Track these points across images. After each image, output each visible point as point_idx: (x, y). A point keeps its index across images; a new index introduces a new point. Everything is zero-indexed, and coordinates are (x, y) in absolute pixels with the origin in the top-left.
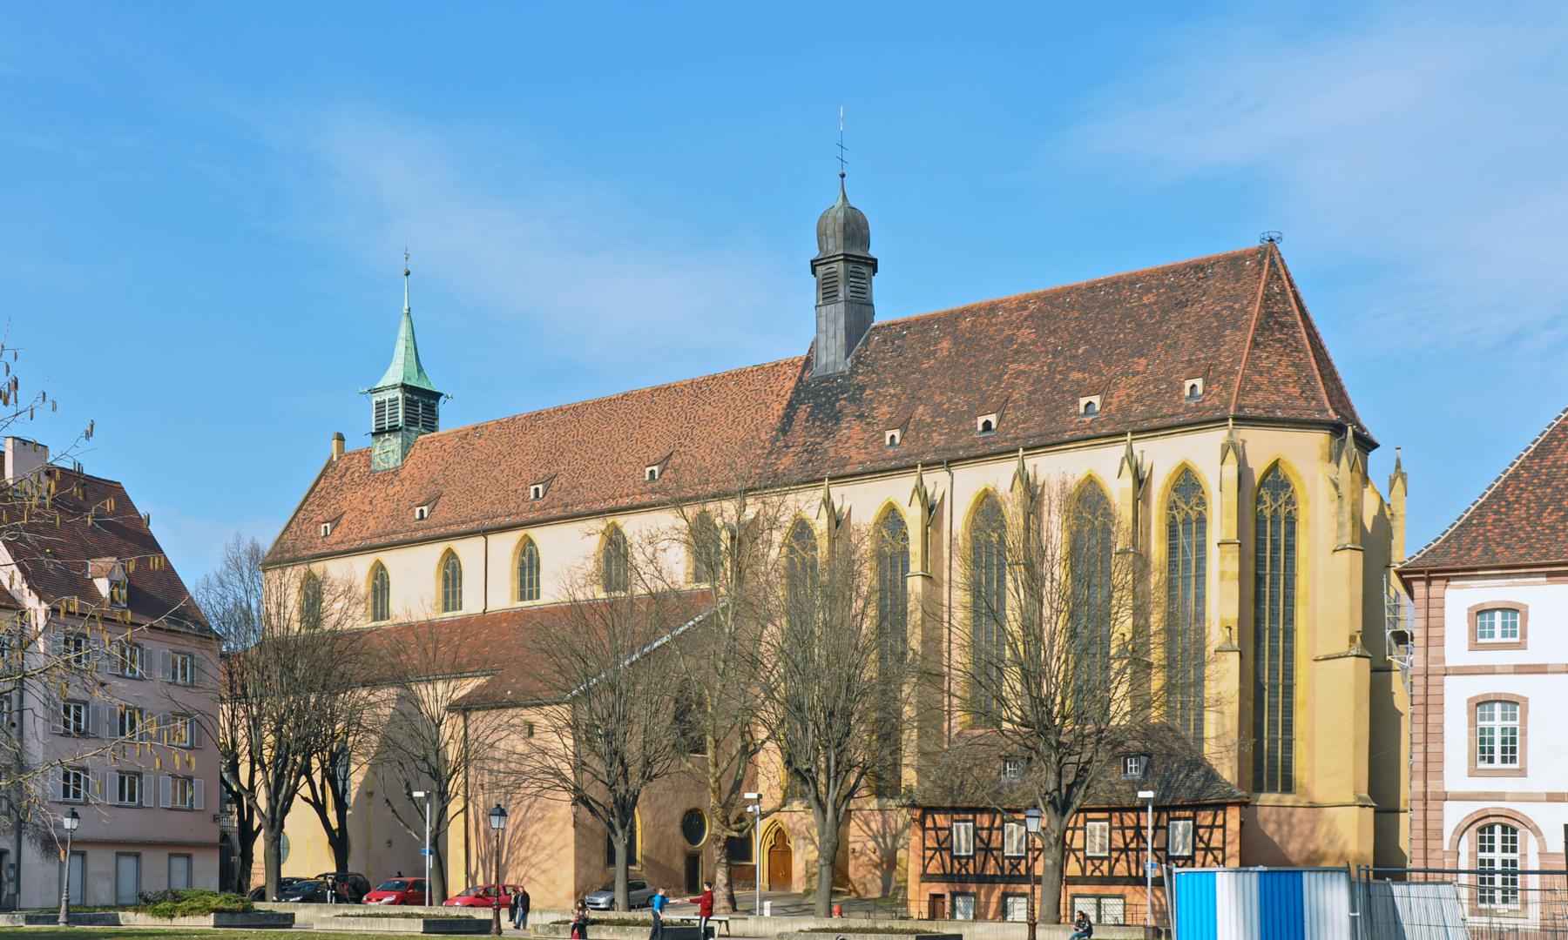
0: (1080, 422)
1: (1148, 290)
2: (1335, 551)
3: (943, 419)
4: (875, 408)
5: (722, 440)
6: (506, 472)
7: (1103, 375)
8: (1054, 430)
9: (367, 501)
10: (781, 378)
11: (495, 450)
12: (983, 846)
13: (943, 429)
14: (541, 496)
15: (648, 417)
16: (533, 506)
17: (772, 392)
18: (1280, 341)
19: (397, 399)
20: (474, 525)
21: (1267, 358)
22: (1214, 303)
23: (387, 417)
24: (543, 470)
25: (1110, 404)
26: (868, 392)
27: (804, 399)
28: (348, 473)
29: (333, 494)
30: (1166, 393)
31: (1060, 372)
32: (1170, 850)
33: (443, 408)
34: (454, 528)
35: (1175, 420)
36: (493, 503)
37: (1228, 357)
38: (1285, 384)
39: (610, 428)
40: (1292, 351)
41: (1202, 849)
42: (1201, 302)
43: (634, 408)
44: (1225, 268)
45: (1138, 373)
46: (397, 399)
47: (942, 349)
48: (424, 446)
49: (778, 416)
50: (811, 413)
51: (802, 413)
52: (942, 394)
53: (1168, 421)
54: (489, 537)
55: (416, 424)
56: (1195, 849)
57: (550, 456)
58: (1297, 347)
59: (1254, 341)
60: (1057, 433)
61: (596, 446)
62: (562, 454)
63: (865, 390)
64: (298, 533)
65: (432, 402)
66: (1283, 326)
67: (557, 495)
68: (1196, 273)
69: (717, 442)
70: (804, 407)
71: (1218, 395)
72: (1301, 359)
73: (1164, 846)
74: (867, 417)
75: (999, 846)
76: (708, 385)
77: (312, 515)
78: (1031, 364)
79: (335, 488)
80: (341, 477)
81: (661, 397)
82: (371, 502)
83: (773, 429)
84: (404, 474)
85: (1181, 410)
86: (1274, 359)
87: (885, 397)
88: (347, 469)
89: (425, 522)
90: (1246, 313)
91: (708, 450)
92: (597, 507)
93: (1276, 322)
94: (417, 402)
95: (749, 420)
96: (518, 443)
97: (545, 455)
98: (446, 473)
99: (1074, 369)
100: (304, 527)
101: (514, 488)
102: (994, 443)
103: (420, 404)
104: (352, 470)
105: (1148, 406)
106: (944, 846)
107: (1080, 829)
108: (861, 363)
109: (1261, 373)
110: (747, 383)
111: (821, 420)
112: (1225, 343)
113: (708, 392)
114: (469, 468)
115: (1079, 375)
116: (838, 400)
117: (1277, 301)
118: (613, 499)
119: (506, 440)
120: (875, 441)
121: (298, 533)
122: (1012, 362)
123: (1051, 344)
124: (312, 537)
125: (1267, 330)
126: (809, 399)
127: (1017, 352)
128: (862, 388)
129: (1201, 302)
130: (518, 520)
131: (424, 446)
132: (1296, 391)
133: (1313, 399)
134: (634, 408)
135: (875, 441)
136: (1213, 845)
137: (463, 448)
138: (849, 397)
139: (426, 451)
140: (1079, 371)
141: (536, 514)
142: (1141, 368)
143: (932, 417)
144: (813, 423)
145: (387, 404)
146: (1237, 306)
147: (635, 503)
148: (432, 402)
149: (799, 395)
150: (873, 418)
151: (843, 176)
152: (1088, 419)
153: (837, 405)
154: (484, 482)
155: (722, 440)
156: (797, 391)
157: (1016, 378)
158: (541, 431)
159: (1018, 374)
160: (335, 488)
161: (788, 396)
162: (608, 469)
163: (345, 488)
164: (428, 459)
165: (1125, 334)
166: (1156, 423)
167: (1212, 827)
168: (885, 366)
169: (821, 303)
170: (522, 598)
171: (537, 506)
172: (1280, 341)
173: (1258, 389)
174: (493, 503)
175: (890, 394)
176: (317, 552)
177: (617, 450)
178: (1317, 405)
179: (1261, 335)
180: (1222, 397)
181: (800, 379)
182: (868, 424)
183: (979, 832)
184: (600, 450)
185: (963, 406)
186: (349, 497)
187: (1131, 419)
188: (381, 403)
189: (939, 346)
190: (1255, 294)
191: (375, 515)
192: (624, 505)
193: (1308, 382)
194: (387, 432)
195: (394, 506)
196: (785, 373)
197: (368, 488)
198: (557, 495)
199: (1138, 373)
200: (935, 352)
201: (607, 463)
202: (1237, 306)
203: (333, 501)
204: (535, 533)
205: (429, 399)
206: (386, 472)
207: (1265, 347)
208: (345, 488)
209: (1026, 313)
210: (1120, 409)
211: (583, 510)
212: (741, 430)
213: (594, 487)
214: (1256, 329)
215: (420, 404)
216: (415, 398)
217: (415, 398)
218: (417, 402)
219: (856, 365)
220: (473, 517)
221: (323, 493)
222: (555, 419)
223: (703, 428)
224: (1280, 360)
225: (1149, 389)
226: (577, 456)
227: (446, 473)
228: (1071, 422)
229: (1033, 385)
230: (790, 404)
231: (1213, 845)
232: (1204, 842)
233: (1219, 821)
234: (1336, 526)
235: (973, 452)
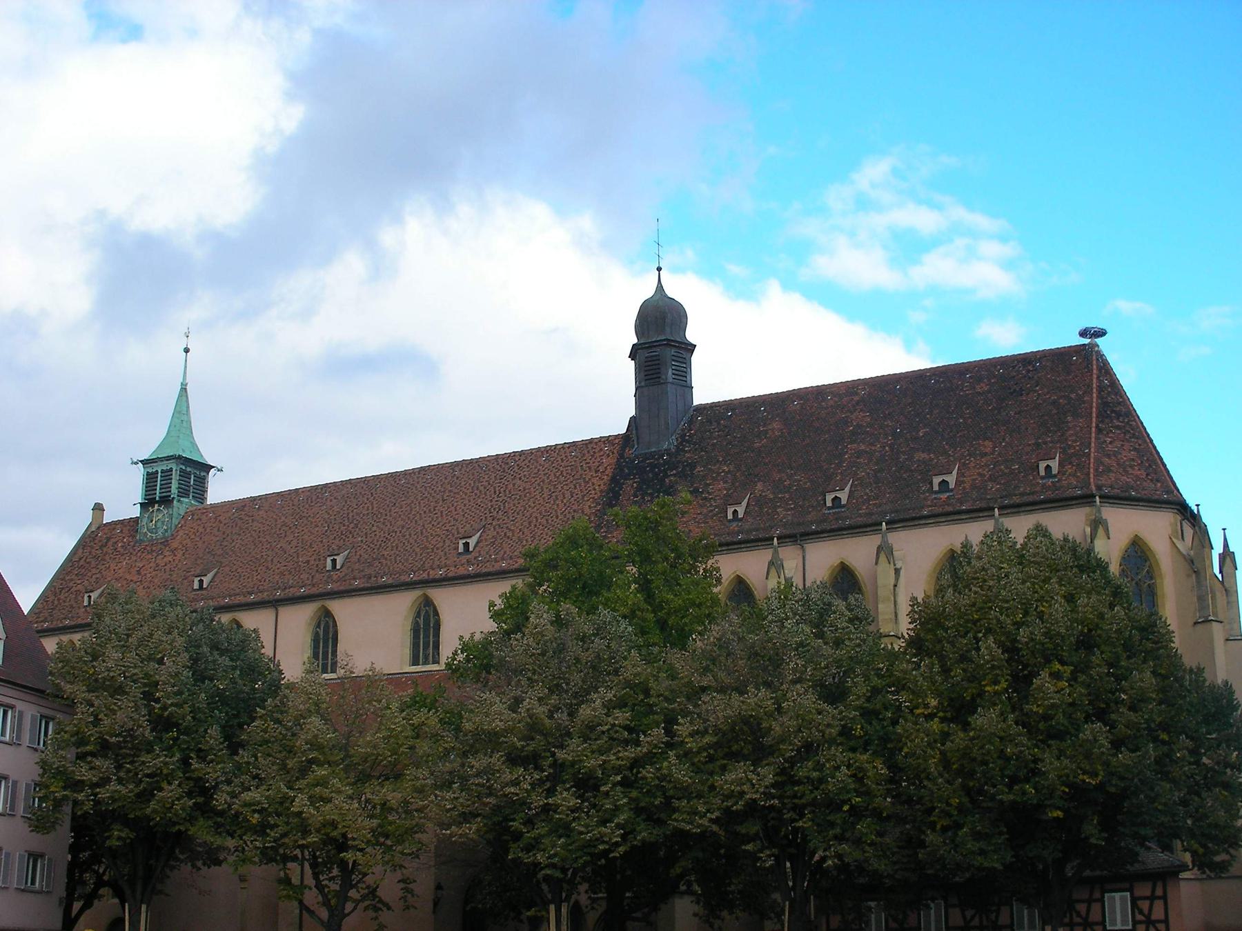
0: (935, 498)
1: (980, 380)
2: (1196, 623)
3: (787, 496)
4: (709, 485)
5: (540, 513)
6: (294, 543)
7: (950, 456)
8: (908, 506)
9: (134, 571)
10: (597, 455)
11: (279, 522)
12: (1143, 918)
13: (787, 504)
14: (338, 567)
15: (450, 491)
16: (329, 577)
17: (590, 468)
18: (1118, 427)
19: (171, 470)
20: (265, 596)
21: (1111, 443)
22: (1048, 393)
23: (158, 489)
24: (337, 542)
25: (963, 482)
26: (699, 469)
27: (629, 475)
28: (110, 543)
29: (93, 563)
30: (1019, 472)
31: (904, 453)
32: (1107, 924)
33: (213, 481)
34: (241, 599)
35: (1035, 498)
36: (282, 574)
37: (1075, 441)
38: (1131, 467)
39: (409, 502)
40: (1130, 437)
41: (1079, 924)
42: (1035, 391)
43: (434, 482)
44: (1053, 361)
45: (986, 454)
46: (171, 470)
47: (773, 430)
48: (196, 517)
49: (601, 491)
50: (639, 489)
51: (630, 486)
52: (779, 471)
53: (1026, 499)
54: (281, 610)
55: (187, 496)
56: (1135, 922)
57: (342, 528)
58: (1134, 434)
59: (1097, 426)
60: (914, 509)
61: (395, 518)
62: (356, 526)
63: (695, 467)
64: (56, 602)
65: (202, 474)
66: (1119, 415)
67: (357, 566)
68: (1024, 366)
69: (534, 515)
70: (630, 482)
71: (1074, 475)
72: (1140, 445)
73: (1101, 919)
74: (702, 493)
75: (1162, 917)
76: (516, 461)
77: (71, 584)
78: (872, 444)
79: (96, 557)
80: (101, 547)
81: (463, 471)
82: (139, 572)
83: (598, 504)
84: (175, 544)
85: (1038, 489)
86: (1118, 444)
87: (719, 474)
88: (108, 539)
89: (204, 592)
90: (1084, 402)
91: (526, 524)
92: (404, 578)
93: (1112, 411)
94: (189, 474)
95: (568, 495)
96: (305, 514)
97: (337, 527)
98: (225, 543)
99: (918, 450)
100: (62, 597)
101: (305, 558)
102: (847, 518)
103: (192, 476)
104: (114, 540)
105: (1003, 484)
106: (972, 924)
107: (1096, 900)
108: (687, 441)
109: (1109, 456)
110: (559, 459)
111: (651, 494)
112: (1069, 428)
113: (516, 468)
114: (252, 539)
115: (924, 456)
116: (666, 476)
117: (1109, 392)
118: (424, 571)
119: (291, 512)
120: (715, 515)
121: (56, 602)
122: (851, 443)
123: (888, 426)
124: (72, 607)
125: (1107, 417)
126: (634, 475)
127: (853, 433)
128: (692, 466)
129: (1035, 391)
130: (314, 591)
131: (196, 517)
132: (1142, 473)
133: (1158, 481)
134: (434, 482)
135: (715, 515)
136: (1153, 917)
137: (241, 519)
138: (678, 473)
139: (198, 522)
140: (923, 452)
141: (335, 585)
142: (988, 450)
143: (774, 493)
144: (643, 498)
145: (160, 474)
146: (1073, 396)
147: (450, 575)
148: (202, 474)
149: (622, 470)
150: (709, 493)
151: (187, 351)
152: (944, 496)
153: (667, 480)
154: (269, 553)
155: (540, 513)
156: (619, 467)
157: (858, 458)
158: (329, 503)
159: (860, 454)
160: (96, 557)
161: (609, 471)
162: (411, 541)
163: (107, 557)
164: (201, 530)
165: (964, 419)
166: (1016, 500)
167: (1152, 898)
168: (713, 445)
169: (643, 384)
170: (415, 662)
171: (335, 577)
172: (1118, 427)
173: (1110, 471)
174: (282, 574)
175: (723, 471)
176: (80, 621)
177: (420, 523)
178: (1161, 486)
179: (1102, 422)
180: (1078, 477)
181: (621, 456)
182: (705, 498)
183: (1139, 903)
184: (400, 523)
185: (805, 483)
186: (113, 566)
187: (988, 497)
188: (152, 473)
189: (770, 427)
190: (1090, 386)
191: (146, 584)
192: (437, 577)
193: (1150, 466)
194: (157, 502)
195: (166, 576)
196: (601, 450)
197: (134, 558)
198: (357, 566)
199: (986, 454)
200: (766, 432)
201: (410, 535)
202: (1073, 396)
203: (94, 571)
204: (336, 607)
205: (200, 470)
206: (152, 543)
207: (1108, 433)
208: (107, 557)
209: (856, 398)
210: (973, 487)
211: (390, 581)
212: (561, 505)
213: (398, 558)
214: (1097, 417)
215: (192, 476)
216: (189, 469)
217: (189, 469)
218: (189, 474)
219: (681, 443)
220: (261, 587)
221: (82, 562)
222: (343, 492)
223: (516, 502)
224: (1122, 445)
225: (1001, 470)
226: (374, 528)
227: (225, 543)
228: (925, 499)
229: (877, 464)
230: (613, 479)
231: (1153, 917)
232: (1144, 915)
233: (1159, 892)
234: (1195, 599)
235: (826, 526)
